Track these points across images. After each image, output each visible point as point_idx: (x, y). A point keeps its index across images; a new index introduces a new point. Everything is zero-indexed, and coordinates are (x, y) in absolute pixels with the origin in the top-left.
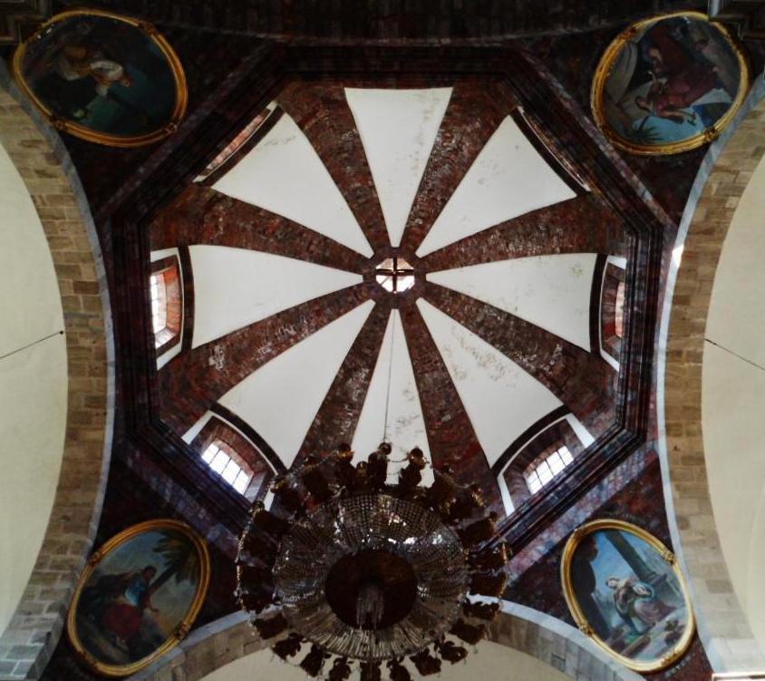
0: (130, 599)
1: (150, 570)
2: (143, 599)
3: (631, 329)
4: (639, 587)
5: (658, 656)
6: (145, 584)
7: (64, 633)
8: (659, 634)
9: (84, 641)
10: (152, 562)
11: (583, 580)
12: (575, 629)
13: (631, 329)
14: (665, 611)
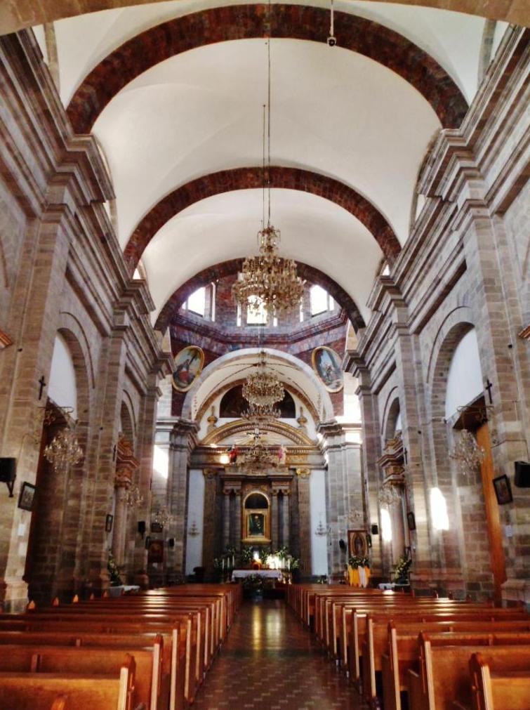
0: (184, 370)
1: (188, 360)
2: (188, 368)
3: (515, 80)
4: (333, 368)
5: (334, 388)
6: (187, 364)
7: (173, 387)
8: (334, 384)
9: (178, 386)
10: (187, 358)
11: (318, 360)
12: (354, 332)
13: (515, 80)
14: (338, 378)
